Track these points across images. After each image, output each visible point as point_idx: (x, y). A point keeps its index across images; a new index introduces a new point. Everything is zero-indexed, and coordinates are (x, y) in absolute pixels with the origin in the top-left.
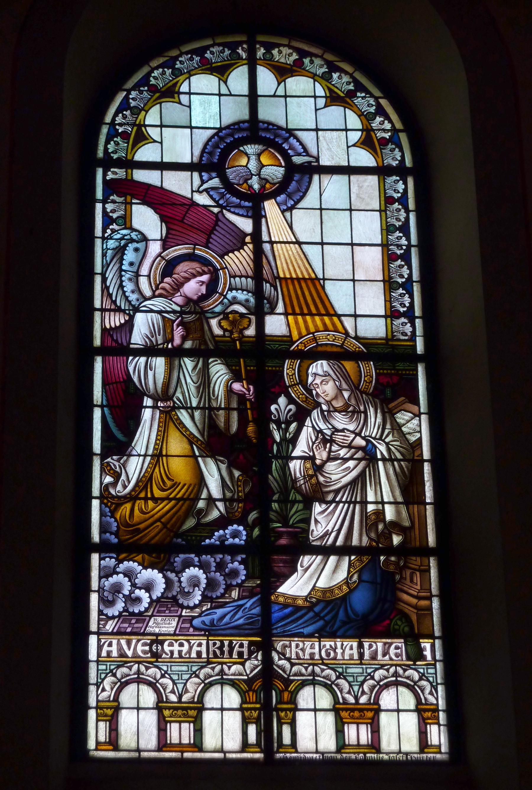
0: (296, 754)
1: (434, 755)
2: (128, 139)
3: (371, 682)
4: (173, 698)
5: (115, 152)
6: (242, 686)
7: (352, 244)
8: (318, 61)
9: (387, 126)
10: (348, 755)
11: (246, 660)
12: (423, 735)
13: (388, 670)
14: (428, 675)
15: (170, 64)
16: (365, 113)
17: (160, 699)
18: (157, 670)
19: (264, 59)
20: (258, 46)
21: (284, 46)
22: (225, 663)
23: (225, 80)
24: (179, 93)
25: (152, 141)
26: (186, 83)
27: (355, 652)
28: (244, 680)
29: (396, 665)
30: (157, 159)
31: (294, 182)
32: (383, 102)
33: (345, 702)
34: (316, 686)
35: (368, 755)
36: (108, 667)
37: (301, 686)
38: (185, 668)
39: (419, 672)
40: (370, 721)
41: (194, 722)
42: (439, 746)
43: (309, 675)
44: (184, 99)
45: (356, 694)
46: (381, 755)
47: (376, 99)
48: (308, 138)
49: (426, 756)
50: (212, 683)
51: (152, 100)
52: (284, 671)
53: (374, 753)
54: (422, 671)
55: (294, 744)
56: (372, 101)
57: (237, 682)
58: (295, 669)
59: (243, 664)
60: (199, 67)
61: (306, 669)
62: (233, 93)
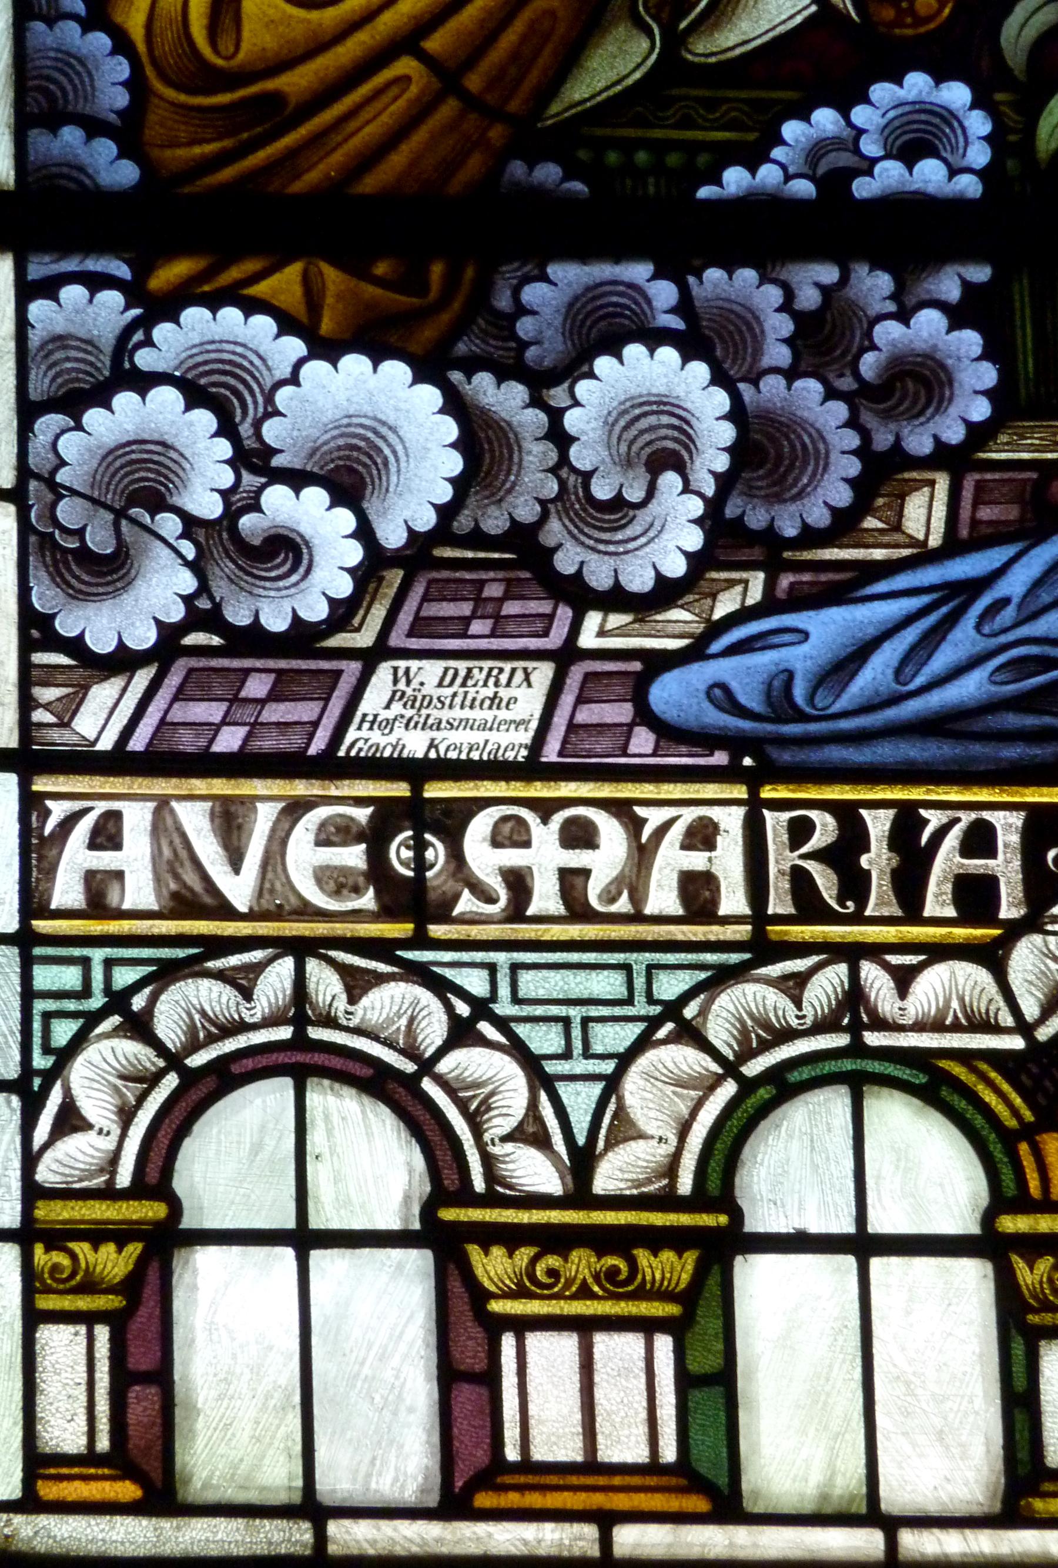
6: (989, 1097)
18: (426, 997)
22: (875, 951)
38: (609, 984)
54: (476, 983)
57: (958, 1070)
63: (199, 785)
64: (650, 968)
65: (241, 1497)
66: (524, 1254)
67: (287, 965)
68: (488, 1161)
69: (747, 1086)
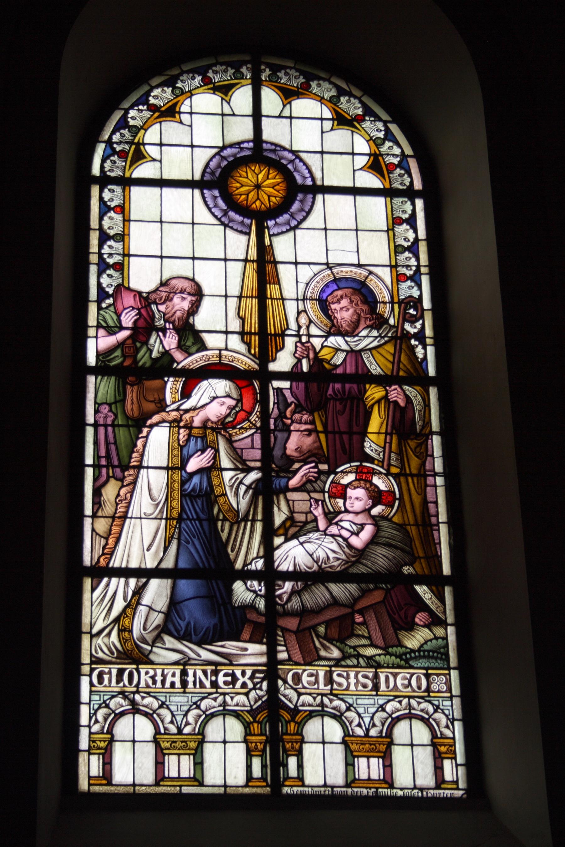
0: (302, 789)
1: (452, 792)
2: (126, 158)
3: (384, 715)
4: (360, 732)
5: (111, 170)
6: (245, 717)
7: (161, 257)
8: (326, 85)
9: (397, 151)
10: (359, 790)
11: (251, 690)
12: (438, 769)
13: (400, 702)
14: (445, 708)
15: (171, 83)
16: (374, 138)
17: (346, 734)
18: (155, 700)
19: (270, 81)
20: (263, 67)
21: (291, 68)
22: (228, 694)
23: (228, 101)
24: (180, 113)
25: (150, 159)
26: (188, 102)
27: (177, 680)
28: (247, 711)
29: (410, 697)
30: (157, 176)
31: (297, 202)
32: (393, 128)
33: (443, 737)
34: (227, 716)
35: (380, 790)
36: (190, 699)
37: (308, 717)
38: (372, 702)
39: (433, 705)
40: (193, 752)
41: (383, 758)
42: (456, 782)
43: (318, 706)
44: (185, 118)
45: (179, 724)
46: (395, 791)
47: (385, 123)
48: (313, 161)
49: (443, 793)
50: (215, 714)
51: (152, 119)
52: (290, 701)
53: (387, 788)
54: (350, 701)
55: (300, 778)
56: (380, 125)
57: (241, 713)
58: (303, 698)
59: (247, 694)
60: (201, 86)
61: (314, 699)
62: (236, 113)
63: (352, 669)
64: (356, 699)
65: (125, 783)
66: (447, 747)
67: (320, 697)
68: (352, 730)
69: (207, 716)
